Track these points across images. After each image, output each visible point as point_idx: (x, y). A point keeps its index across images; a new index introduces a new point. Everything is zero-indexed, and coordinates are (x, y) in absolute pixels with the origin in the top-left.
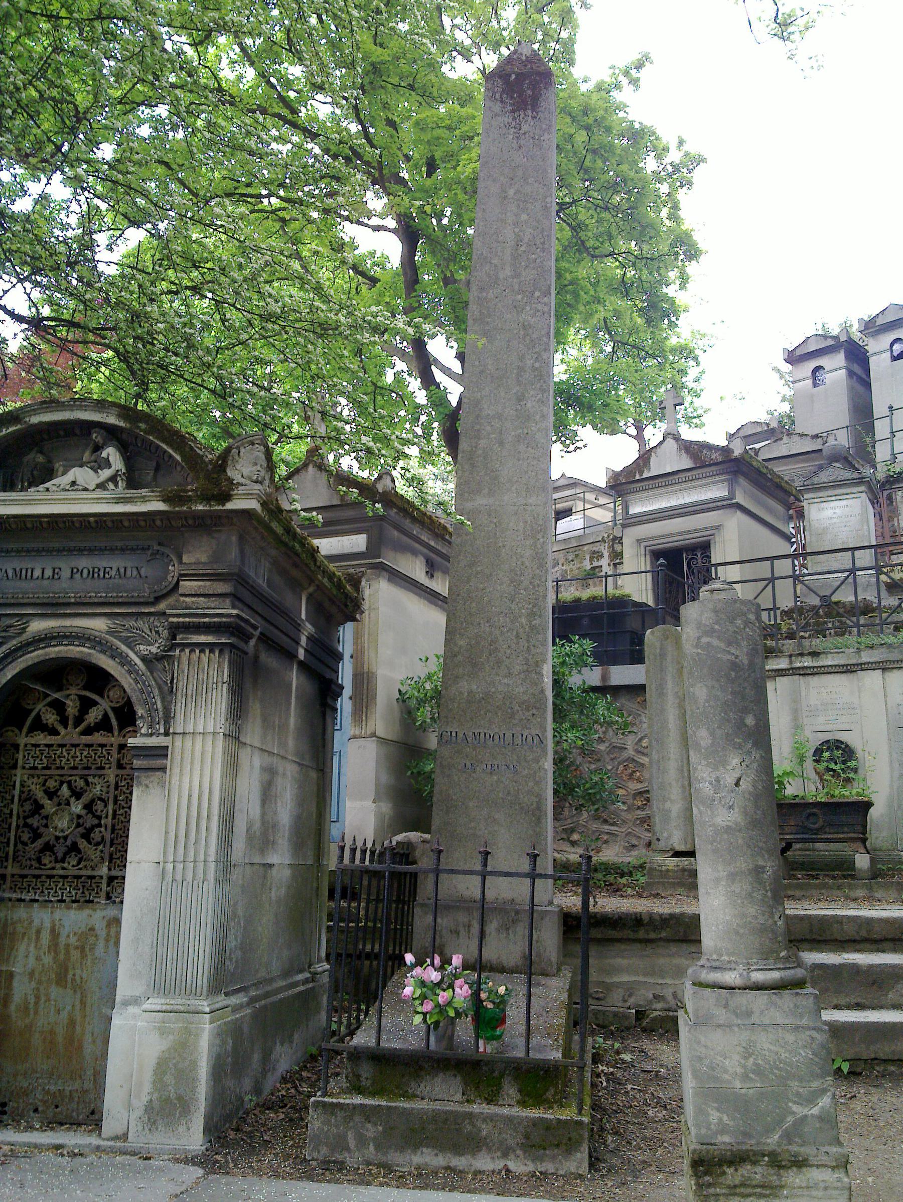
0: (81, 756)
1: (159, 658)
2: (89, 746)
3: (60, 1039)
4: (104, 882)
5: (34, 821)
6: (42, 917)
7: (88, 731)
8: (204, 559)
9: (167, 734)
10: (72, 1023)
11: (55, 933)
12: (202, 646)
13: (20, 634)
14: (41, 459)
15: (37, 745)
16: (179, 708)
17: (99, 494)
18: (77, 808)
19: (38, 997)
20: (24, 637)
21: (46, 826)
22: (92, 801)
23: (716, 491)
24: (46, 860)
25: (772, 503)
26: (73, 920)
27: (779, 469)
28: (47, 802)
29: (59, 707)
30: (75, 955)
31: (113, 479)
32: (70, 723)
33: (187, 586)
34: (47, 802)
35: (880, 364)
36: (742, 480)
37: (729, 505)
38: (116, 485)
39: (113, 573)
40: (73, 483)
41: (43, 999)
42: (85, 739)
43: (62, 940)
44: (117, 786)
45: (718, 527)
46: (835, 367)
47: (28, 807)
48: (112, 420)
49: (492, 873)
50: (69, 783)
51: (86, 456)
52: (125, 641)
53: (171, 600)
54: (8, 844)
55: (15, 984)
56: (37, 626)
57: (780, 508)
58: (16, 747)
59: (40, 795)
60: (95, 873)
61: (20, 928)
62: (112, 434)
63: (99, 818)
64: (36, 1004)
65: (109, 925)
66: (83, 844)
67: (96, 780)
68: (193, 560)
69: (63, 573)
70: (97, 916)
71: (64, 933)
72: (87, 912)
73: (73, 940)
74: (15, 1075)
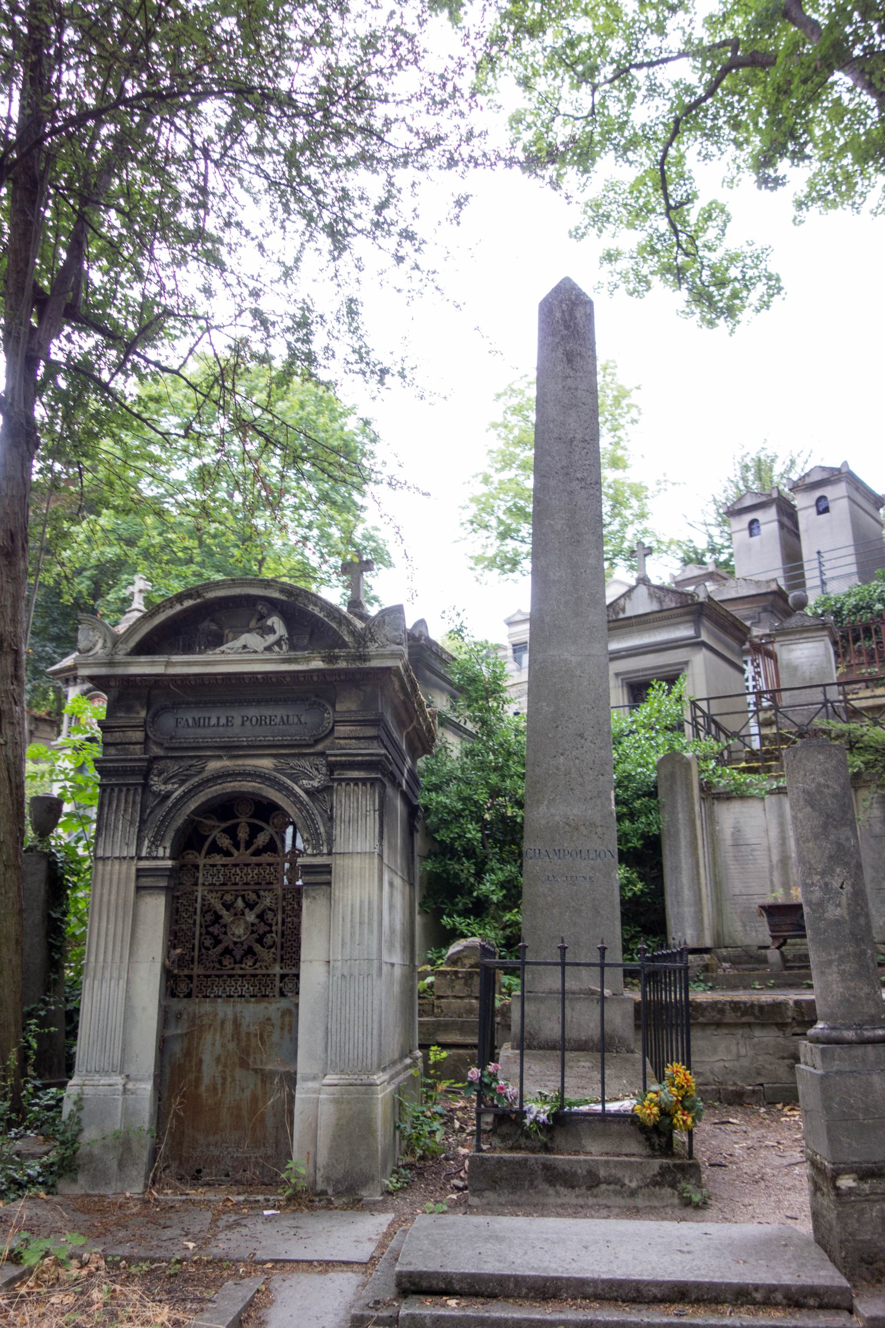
0: (252, 874)
1: (318, 790)
2: (259, 865)
3: (244, 1113)
4: (278, 979)
5: (215, 930)
6: (224, 1010)
7: (258, 853)
8: (354, 707)
9: (330, 853)
10: (255, 1099)
11: (237, 1024)
12: (356, 781)
13: (200, 773)
14: (214, 627)
15: (213, 866)
16: (337, 832)
17: (268, 656)
19: (224, 1079)
20: (204, 775)
21: (225, 933)
22: (263, 911)
23: (685, 632)
24: (225, 963)
25: (729, 640)
26: (251, 1012)
27: (730, 608)
28: (224, 912)
29: (231, 832)
30: (255, 1042)
31: (278, 643)
32: (242, 846)
33: (342, 730)
34: (224, 912)
35: (807, 518)
36: (706, 622)
37: (697, 644)
38: (281, 647)
39: (278, 720)
40: (245, 647)
41: (229, 1080)
42: (255, 859)
43: (244, 1029)
44: (284, 898)
45: (686, 663)
46: (769, 519)
47: (209, 917)
48: (276, 595)
49: (609, 965)
50: (243, 897)
52: (290, 776)
53: (327, 742)
54: (193, 949)
55: (204, 1067)
56: (213, 766)
57: (734, 644)
58: (197, 867)
59: (218, 906)
60: (270, 972)
61: (206, 1021)
62: (274, 606)
63: (270, 925)
64: (223, 1084)
65: (283, 1015)
66: (257, 948)
67: (266, 894)
68: (344, 708)
69: (236, 723)
70: (274, 1007)
71: (244, 1023)
72: (264, 1005)
73: (252, 1029)
74: (208, 1145)
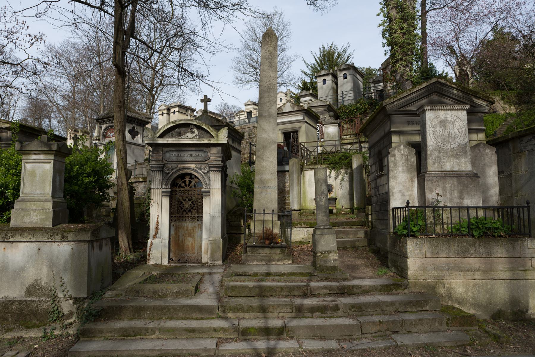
5: (181, 206)
10: (192, 244)
18: (190, 203)
23: (300, 117)
31: (196, 136)
33: (212, 158)
47: (180, 203)
51: (189, 130)
52: (199, 169)
59: (182, 200)
66: (192, 210)
